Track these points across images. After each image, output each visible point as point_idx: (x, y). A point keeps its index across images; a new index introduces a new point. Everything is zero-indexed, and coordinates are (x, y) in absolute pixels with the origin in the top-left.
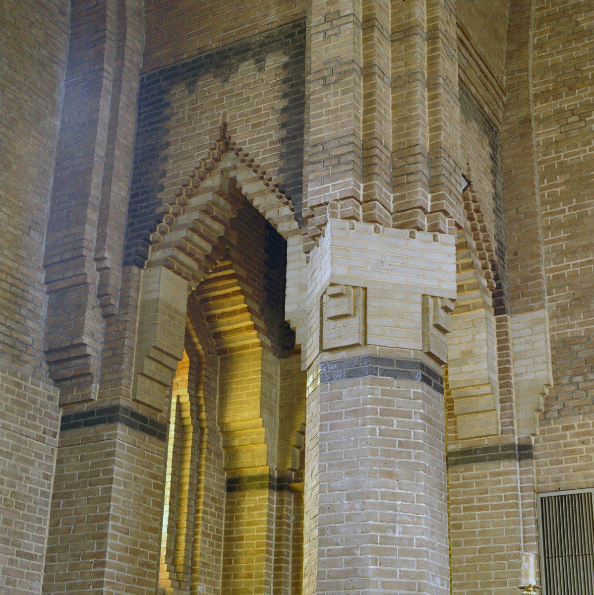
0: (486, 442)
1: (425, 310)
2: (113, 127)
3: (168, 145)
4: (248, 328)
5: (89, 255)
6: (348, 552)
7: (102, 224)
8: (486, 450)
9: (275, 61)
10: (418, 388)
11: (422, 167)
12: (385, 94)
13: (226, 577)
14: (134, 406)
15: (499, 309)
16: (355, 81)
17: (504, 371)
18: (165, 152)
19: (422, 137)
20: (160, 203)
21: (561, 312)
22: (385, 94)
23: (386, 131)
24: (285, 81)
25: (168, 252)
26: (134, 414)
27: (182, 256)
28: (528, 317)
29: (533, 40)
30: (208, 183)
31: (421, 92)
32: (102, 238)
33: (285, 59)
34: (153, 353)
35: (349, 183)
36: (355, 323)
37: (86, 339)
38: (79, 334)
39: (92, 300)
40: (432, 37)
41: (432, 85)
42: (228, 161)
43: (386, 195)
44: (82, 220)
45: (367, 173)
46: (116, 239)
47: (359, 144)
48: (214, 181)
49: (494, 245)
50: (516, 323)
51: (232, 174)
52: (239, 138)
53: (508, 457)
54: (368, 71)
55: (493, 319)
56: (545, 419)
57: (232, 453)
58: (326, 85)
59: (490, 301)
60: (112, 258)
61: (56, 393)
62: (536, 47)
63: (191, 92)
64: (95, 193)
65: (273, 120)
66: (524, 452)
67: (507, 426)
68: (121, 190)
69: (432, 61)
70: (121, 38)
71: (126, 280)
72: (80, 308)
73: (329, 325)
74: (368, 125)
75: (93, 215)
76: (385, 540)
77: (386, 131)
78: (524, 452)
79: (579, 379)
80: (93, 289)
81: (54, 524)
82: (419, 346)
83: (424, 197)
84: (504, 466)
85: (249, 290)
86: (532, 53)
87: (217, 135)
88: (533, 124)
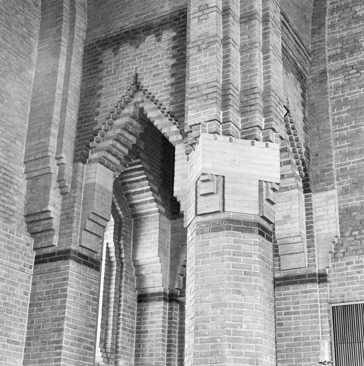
0: (299, 272)
1: (261, 190)
2: (67, 76)
3: (101, 87)
4: (151, 201)
5: (52, 155)
6: (213, 340)
7: (60, 136)
8: (298, 277)
10: (256, 238)
11: (259, 101)
12: (236, 56)
13: (137, 356)
14: (80, 250)
15: (307, 189)
16: (218, 46)
17: (309, 228)
18: (100, 92)
19: (259, 82)
20: (96, 123)
21: (345, 191)
22: (236, 56)
23: (236, 78)
24: (174, 48)
25: (102, 154)
26: (80, 255)
27: (110, 157)
28: (324, 194)
29: (328, 23)
30: (126, 111)
31: (258, 54)
32: (60, 145)
33: (174, 34)
34: (92, 217)
35: (215, 111)
36: (218, 198)
37: (50, 208)
38: (46, 205)
39: (54, 183)
40: (266, 20)
41: (265, 51)
42: (138, 98)
43: (236, 117)
44: (48, 134)
45: (225, 105)
46: (69, 146)
47: (220, 86)
48: (130, 110)
49: (304, 150)
50: (317, 198)
51: (141, 105)
52: (145, 83)
53: (312, 281)
54: (226, 42)
55: (303, 195)
56: (335, 258)
57: (140, 278)
58: (199, 50)
59: (301, 185)
60: (67, 158)
61: (32, 241)
62: (330, 27)
63: (116, 55)
64: (56, 117)
65: (167, 72)
66: (322, 278)
67: (312, 262)
68: (72, 116)
69: (265, 35)
70: (72, 21)
71: (75, 171)
72: (47, 188)
73: (200, 199)
74: (226, 75)
75: (54, 131)
76: (236, 333)
77: (236, 78)
78: (322, 278)
79: (356, 233)
80: (55, 177)
81: (31, 323)
82: (257, 212)
83: (259, 120)
84: (309, 287)
85: (151, 178)
86: (327, 31)
87: (132, 81)
88: (328, 75)
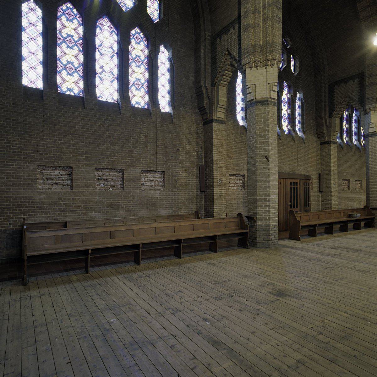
9: (356, 80)
